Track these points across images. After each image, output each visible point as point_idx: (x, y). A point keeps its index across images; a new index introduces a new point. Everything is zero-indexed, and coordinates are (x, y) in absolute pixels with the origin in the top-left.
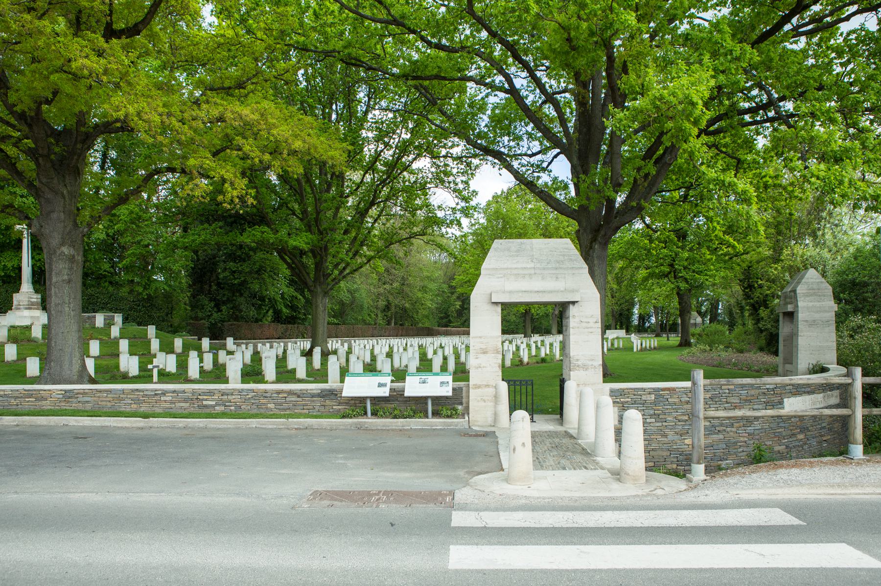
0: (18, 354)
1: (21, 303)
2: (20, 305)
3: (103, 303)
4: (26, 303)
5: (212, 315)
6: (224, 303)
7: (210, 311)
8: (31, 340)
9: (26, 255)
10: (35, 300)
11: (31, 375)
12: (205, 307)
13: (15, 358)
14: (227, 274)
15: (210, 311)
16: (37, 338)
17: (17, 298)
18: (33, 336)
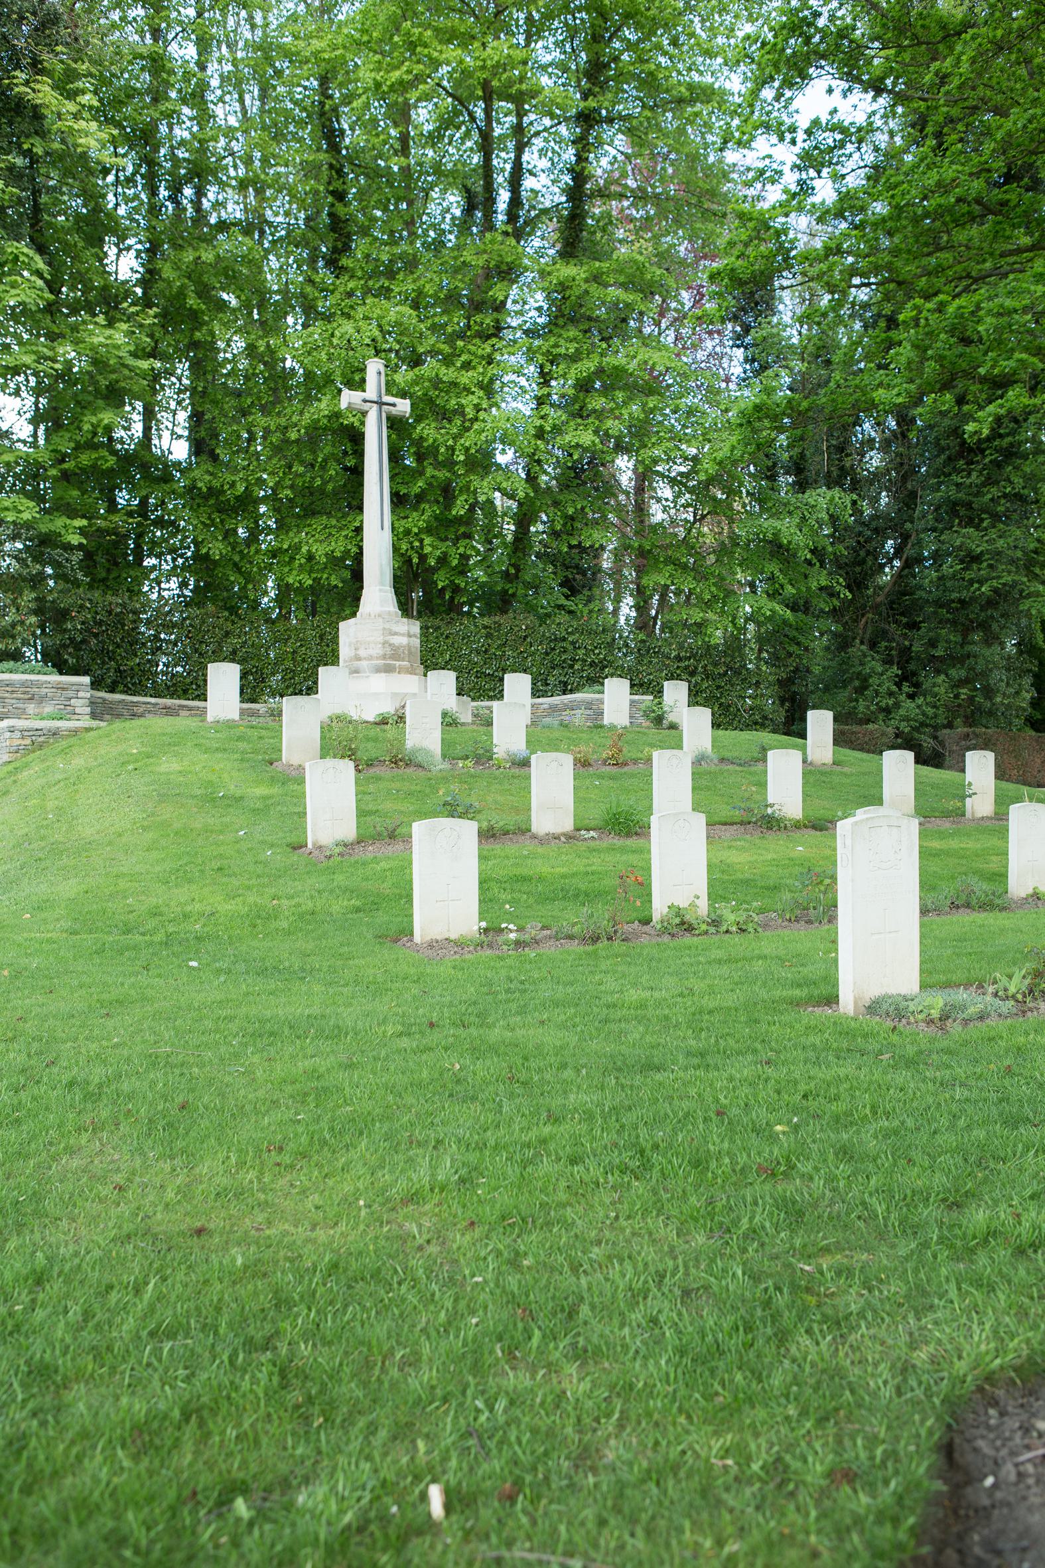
0: (362, 813)
1: (362, 653)
2: (358, 659)
3: (593, 664)
4: (377, 651)
5: (897, 705)
6: (939, 665)
7: (891, 694)
8: (401, 760)
9: (376, 489)
10: (404, 641)
11: (438, 932)
12: (874, 681)
13: (348, 830)
14: (950, 566)
15: (891, 694)
16: (427, 752)
17: (348, 631)
18: (409, 744)
